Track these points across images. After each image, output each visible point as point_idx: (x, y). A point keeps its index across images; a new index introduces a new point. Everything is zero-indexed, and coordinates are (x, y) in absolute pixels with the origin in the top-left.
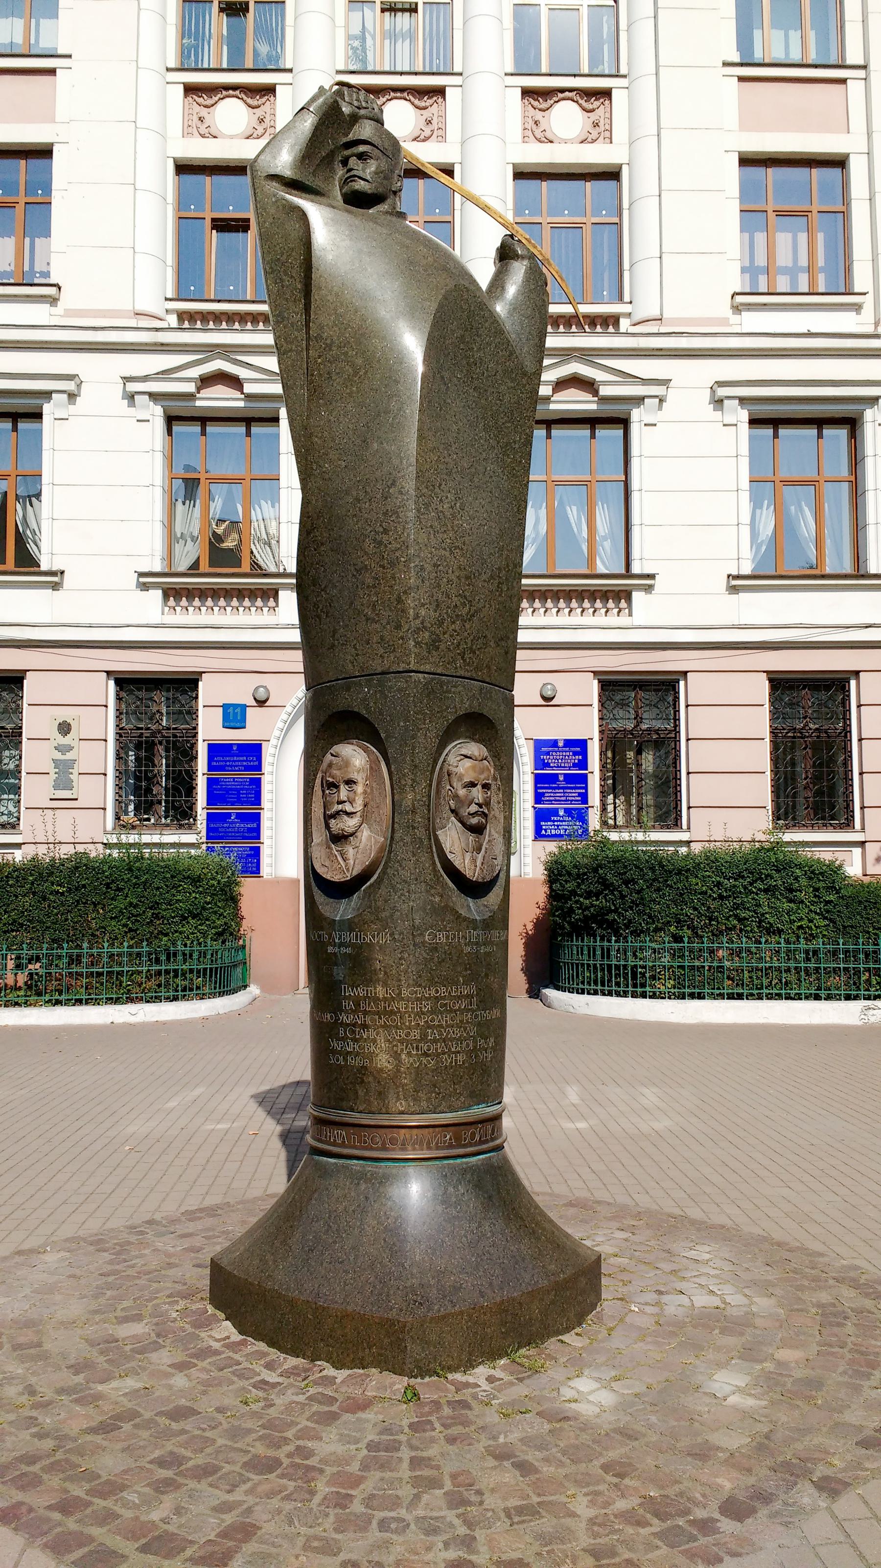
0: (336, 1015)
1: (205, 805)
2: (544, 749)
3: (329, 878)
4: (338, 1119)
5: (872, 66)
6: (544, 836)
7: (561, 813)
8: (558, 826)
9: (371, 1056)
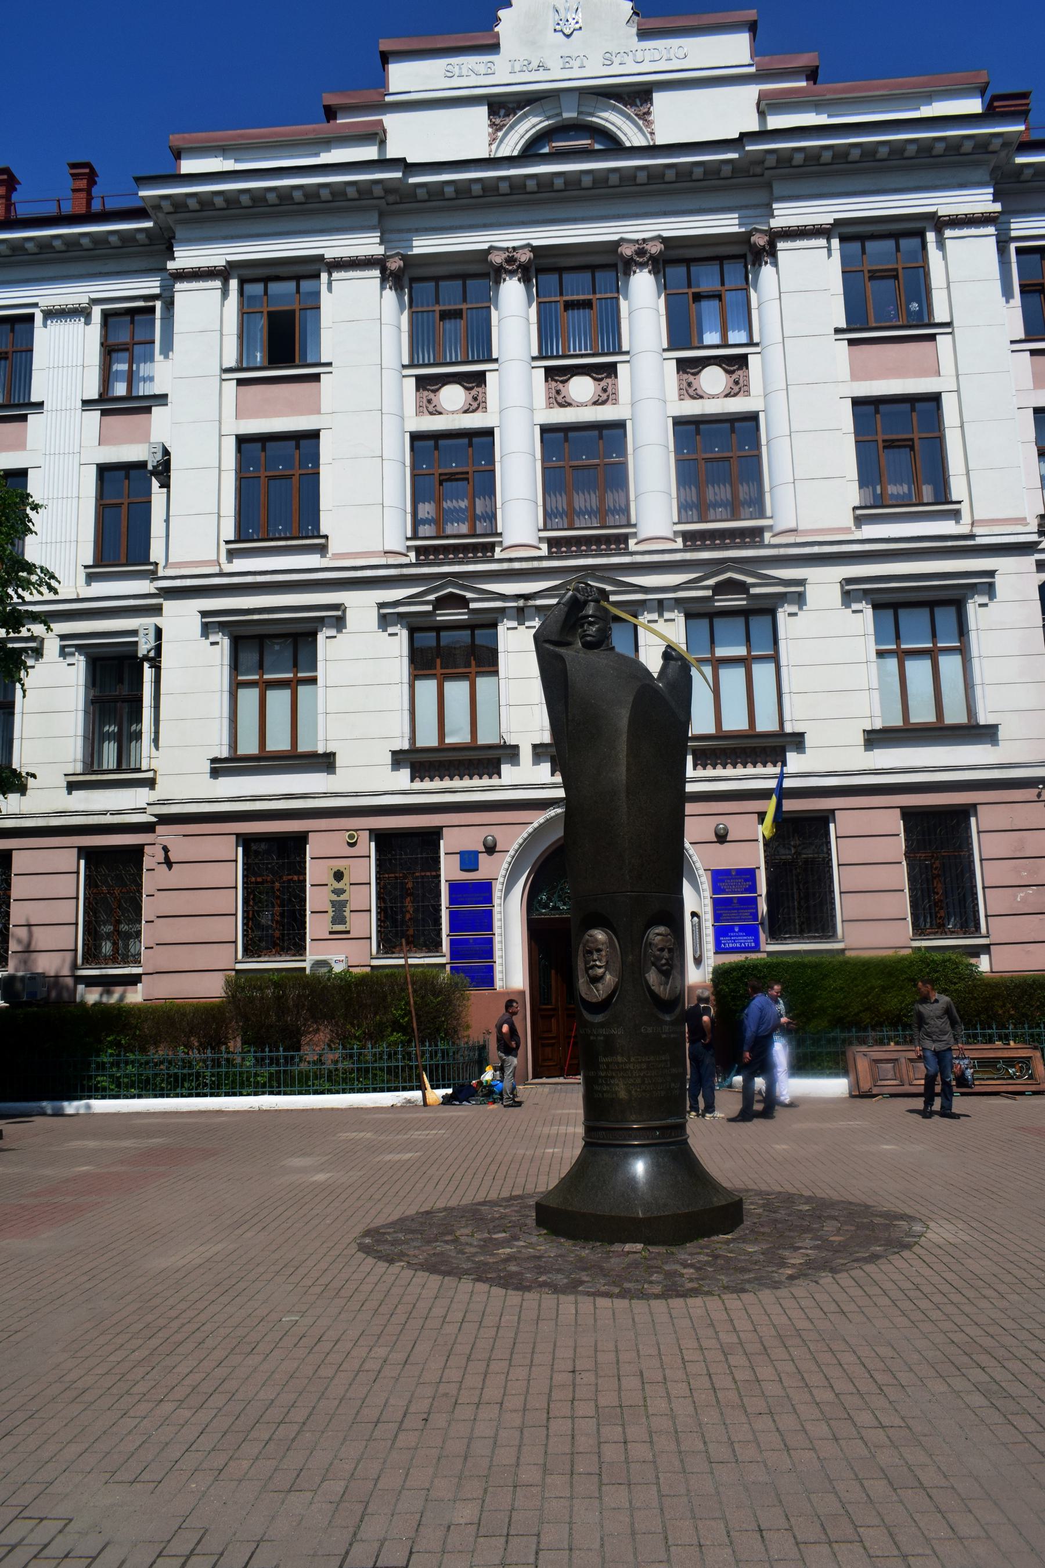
2: (720, 878)
5: (955, 324)
7: (737, 929)
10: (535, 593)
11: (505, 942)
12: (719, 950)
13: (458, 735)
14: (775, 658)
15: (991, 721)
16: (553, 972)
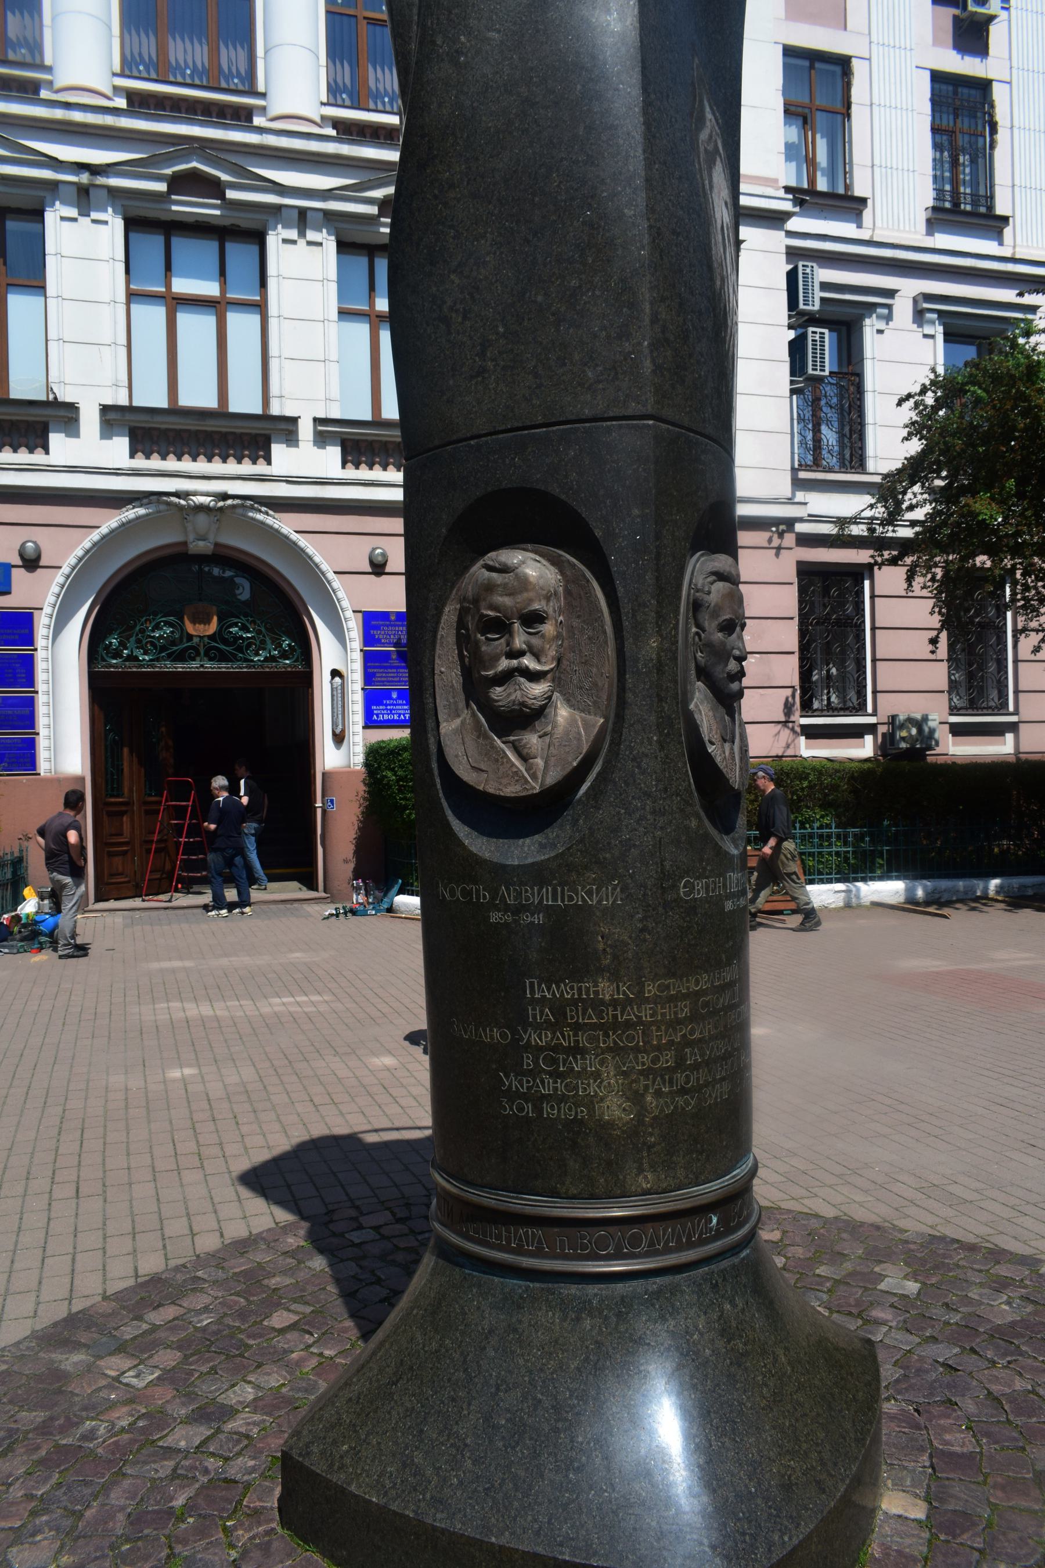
0: (514, 1032)
3: (491, 791)
4: (528, 1210)
6: (376, 721)
7: (394, 695)
8: (391, 710)
9: (591, 1102)
10: (108, 165)
11: (54, 704)
12: (370, 723)
14: (260, 307)
15: (289, 413)
16: (126, 750)
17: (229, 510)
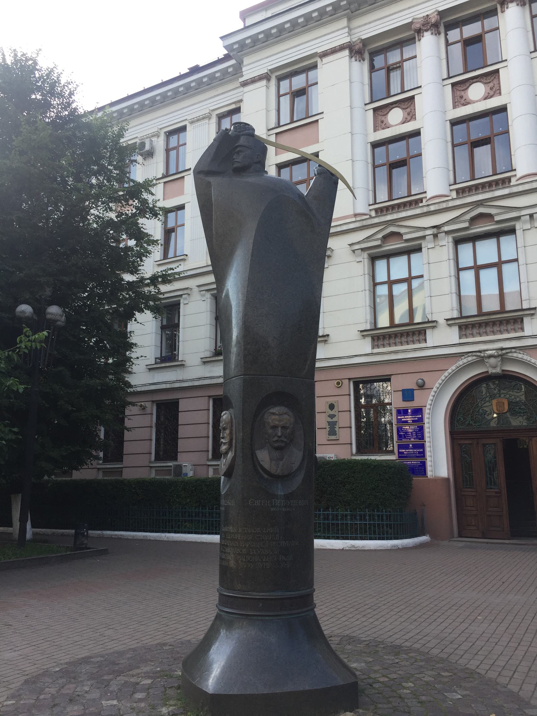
1: (396, 440)
13: (491, 305)
17: (503, 355)
